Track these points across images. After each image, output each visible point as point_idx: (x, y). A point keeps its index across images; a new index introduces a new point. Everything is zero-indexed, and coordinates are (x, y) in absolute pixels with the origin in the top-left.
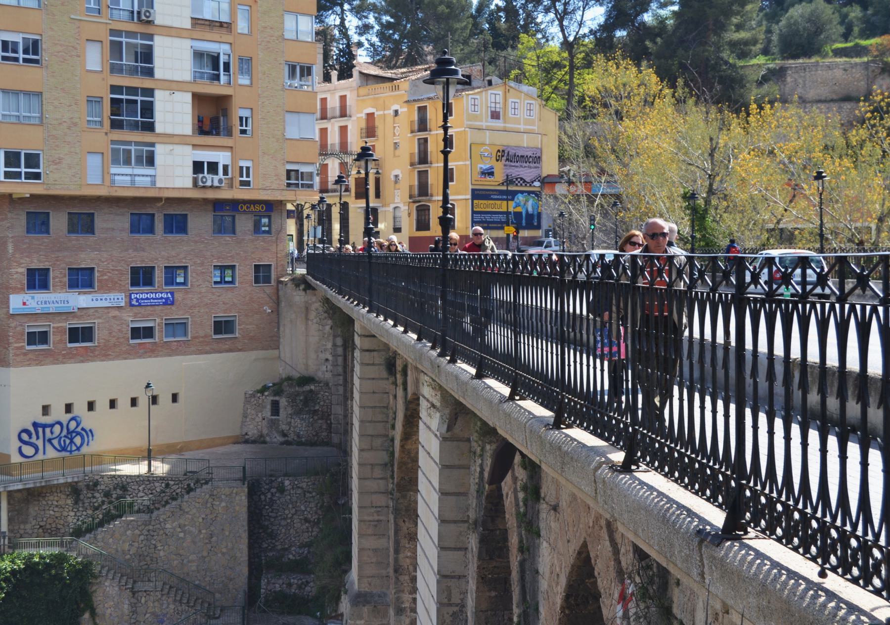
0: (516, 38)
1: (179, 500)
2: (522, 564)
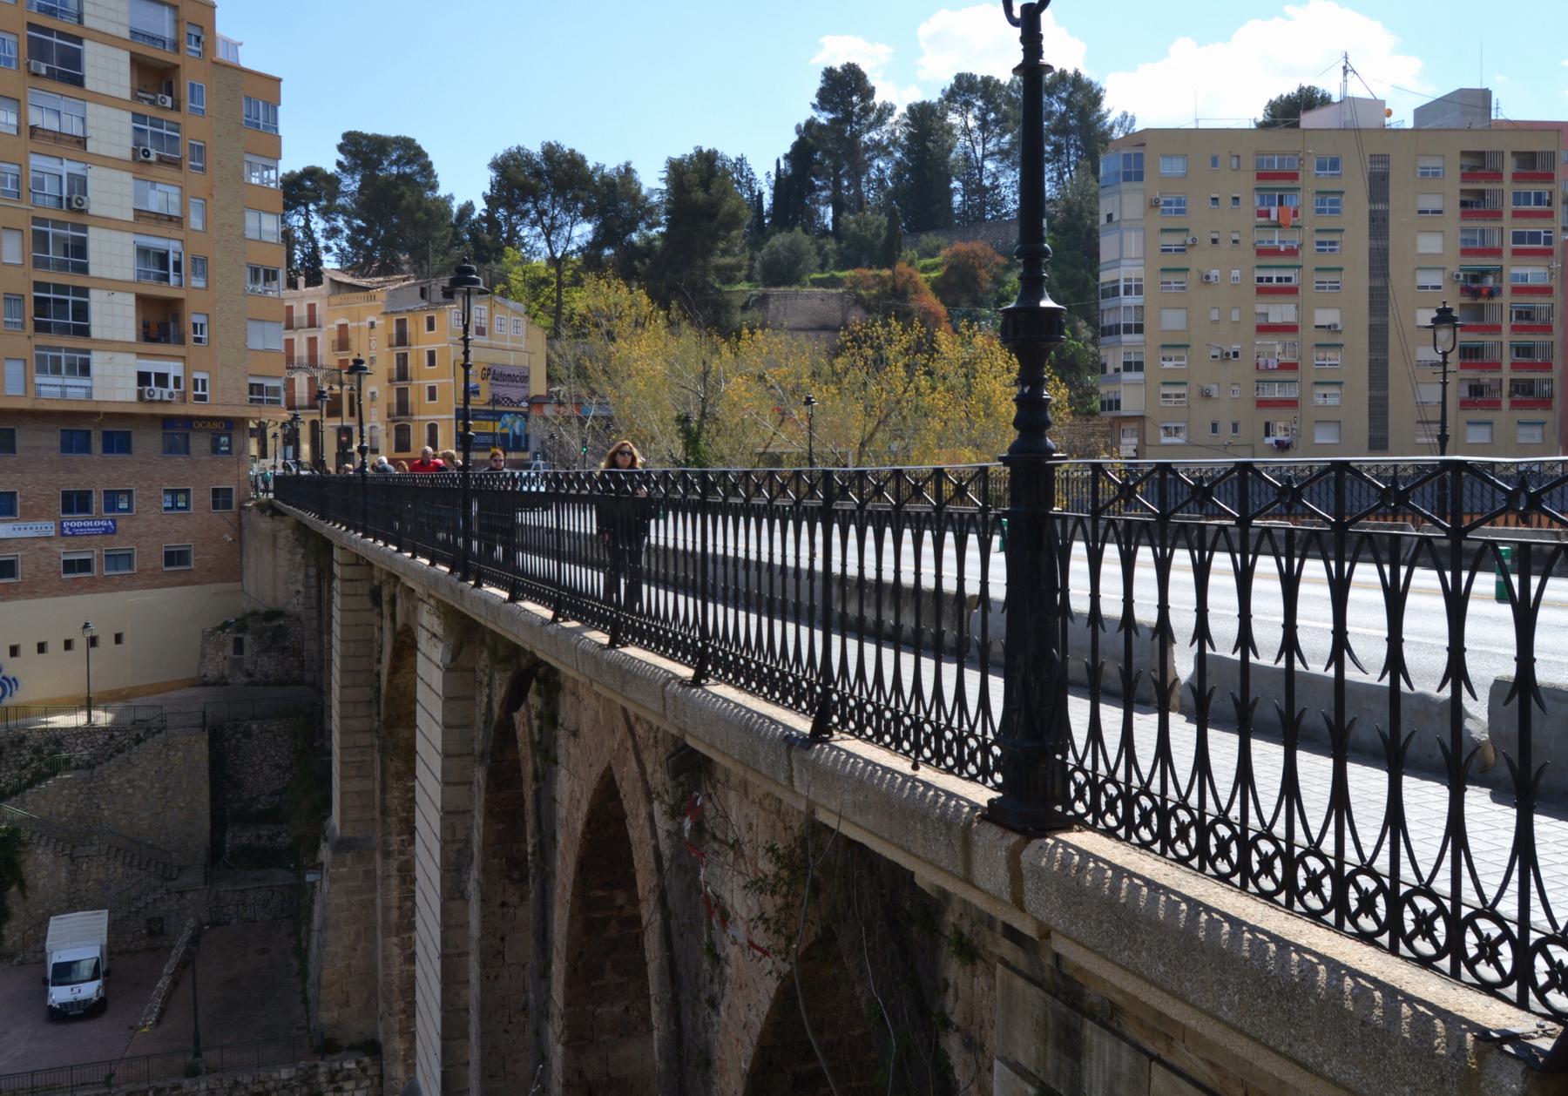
0: (500, 252)
1: (127, 752)
2: (537, 793)
